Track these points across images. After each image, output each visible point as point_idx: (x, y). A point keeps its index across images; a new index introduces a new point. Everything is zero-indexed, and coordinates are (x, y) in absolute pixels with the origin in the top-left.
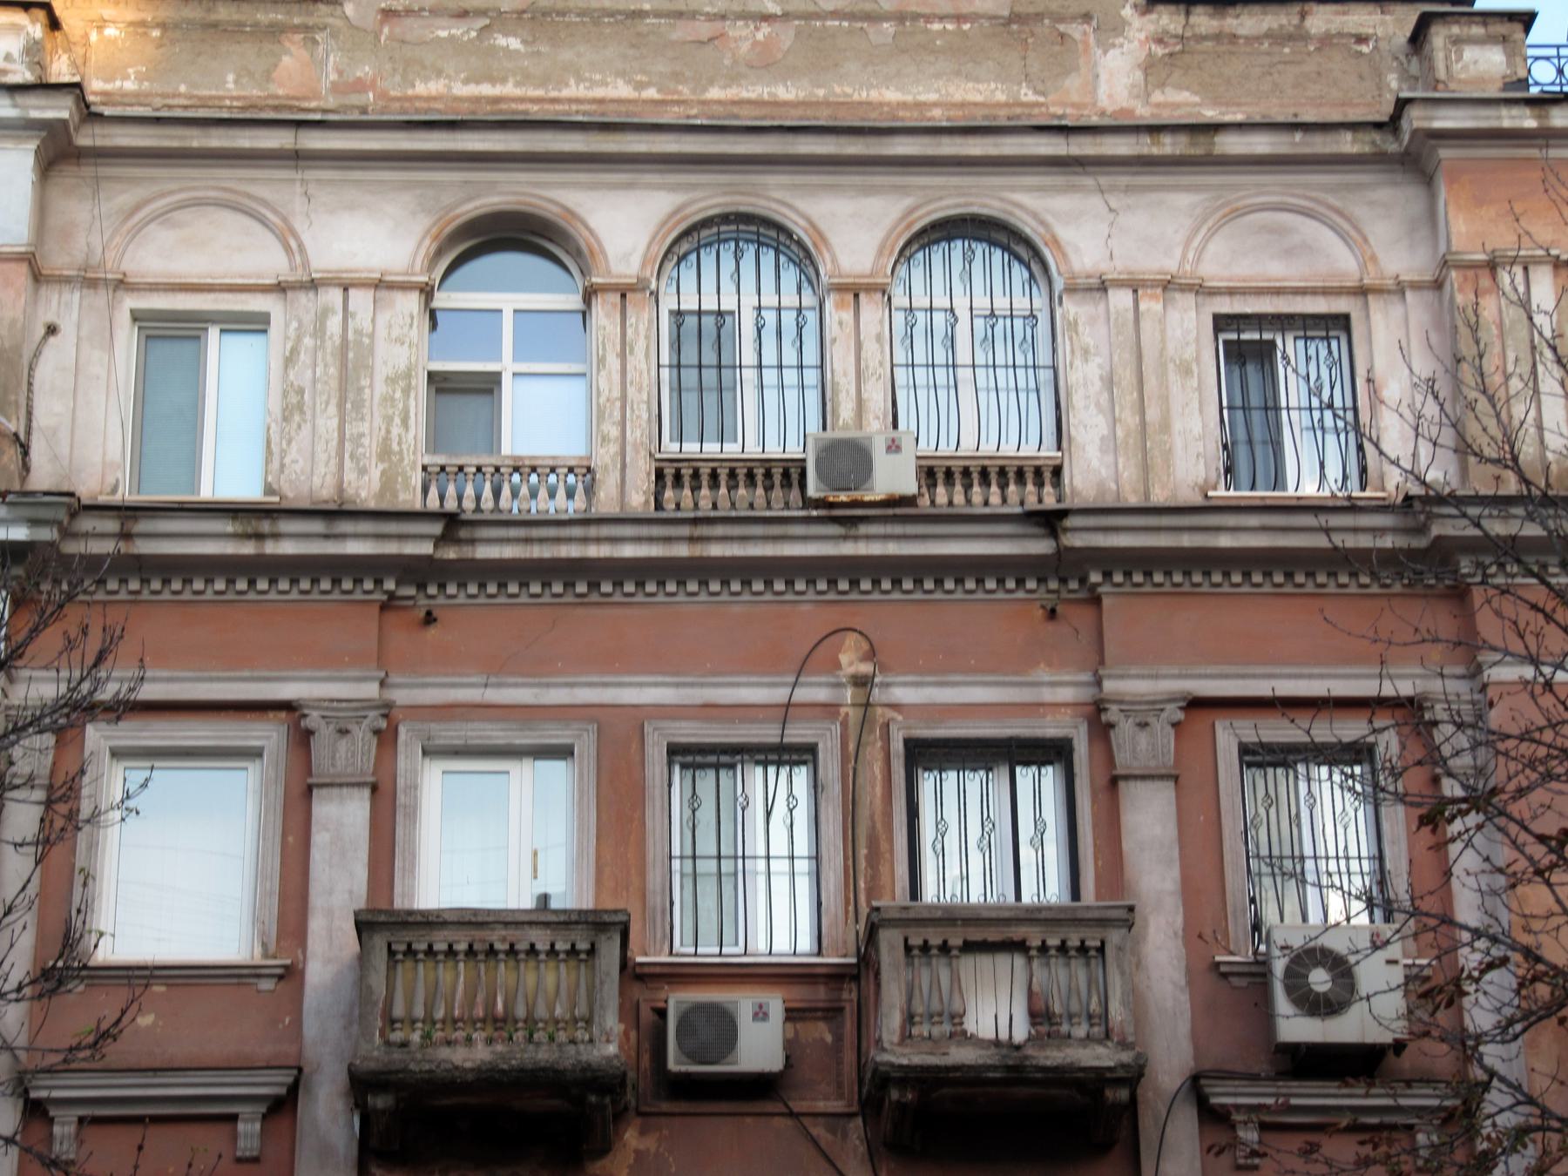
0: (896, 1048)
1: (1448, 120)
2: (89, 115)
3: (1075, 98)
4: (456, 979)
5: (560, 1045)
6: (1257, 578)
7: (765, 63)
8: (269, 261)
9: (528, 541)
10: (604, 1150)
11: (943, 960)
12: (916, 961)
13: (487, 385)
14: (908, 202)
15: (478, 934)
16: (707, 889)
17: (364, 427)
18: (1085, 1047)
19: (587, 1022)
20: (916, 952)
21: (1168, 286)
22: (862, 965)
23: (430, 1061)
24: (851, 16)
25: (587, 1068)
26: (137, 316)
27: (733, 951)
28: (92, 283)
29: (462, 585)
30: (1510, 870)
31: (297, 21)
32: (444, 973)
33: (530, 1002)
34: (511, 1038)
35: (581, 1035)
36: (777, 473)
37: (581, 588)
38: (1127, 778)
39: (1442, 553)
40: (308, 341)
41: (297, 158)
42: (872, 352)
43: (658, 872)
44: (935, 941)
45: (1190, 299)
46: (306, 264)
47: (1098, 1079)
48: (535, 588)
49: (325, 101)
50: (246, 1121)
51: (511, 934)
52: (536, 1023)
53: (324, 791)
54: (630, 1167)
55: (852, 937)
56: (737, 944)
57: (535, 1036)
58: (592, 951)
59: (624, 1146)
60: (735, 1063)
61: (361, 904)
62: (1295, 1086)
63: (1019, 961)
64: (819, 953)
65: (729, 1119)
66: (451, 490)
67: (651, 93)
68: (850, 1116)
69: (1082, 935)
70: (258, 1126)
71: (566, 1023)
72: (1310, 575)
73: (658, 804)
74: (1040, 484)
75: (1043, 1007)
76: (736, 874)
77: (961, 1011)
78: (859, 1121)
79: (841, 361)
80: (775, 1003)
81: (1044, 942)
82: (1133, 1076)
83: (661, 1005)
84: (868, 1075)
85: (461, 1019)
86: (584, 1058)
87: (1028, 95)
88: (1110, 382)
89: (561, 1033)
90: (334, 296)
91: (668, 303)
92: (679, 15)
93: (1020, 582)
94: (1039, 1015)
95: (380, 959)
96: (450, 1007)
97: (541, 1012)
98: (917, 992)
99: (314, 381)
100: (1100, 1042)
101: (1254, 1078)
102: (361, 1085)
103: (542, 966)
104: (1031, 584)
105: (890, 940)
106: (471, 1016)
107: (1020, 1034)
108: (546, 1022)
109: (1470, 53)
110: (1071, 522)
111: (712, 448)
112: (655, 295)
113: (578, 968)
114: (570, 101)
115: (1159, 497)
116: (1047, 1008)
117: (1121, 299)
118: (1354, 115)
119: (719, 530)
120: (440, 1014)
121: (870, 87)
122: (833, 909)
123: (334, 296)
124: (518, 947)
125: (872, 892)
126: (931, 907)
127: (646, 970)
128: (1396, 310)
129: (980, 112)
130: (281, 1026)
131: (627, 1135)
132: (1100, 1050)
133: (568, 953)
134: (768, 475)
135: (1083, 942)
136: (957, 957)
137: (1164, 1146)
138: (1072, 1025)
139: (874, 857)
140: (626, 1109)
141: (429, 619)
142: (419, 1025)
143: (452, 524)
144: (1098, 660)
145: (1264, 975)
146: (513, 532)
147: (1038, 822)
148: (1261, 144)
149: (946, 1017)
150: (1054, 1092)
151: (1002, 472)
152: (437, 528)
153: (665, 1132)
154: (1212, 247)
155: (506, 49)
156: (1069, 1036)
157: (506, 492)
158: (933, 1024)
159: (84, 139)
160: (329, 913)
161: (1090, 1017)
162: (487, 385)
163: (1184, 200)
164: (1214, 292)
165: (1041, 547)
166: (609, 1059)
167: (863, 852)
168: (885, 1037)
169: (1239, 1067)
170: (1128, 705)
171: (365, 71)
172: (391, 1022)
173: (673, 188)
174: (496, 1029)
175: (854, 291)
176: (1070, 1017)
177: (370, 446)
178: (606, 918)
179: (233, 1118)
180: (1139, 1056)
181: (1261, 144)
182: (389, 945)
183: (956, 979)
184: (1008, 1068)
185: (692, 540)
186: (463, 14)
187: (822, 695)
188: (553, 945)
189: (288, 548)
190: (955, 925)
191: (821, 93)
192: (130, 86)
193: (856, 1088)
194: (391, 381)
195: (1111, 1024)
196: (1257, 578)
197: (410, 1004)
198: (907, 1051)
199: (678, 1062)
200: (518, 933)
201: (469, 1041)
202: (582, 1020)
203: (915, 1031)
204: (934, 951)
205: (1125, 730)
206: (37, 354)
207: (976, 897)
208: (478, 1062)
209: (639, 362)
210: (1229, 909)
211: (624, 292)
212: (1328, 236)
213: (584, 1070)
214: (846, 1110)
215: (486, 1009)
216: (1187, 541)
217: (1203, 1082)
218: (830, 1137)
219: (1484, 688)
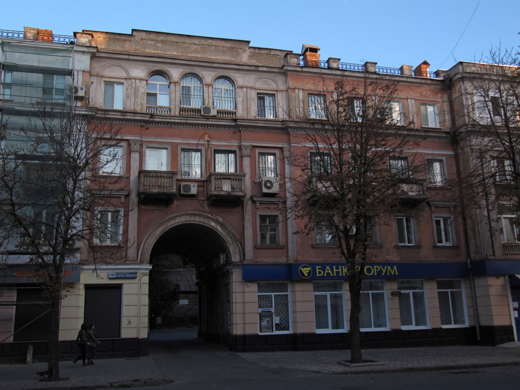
1: (290, 68)
2: (98, 51)
3: (239, 60)
4: (153, 180)
6: (262, 130)
7: (196, 51)
8: (124, 75)
9: (162, 118)
10: (172, 204)
13: (155, 95)
14: (216, 73)
15: (156, 174)
17: (138, 100)
21: (251, 88)
24: (208, 45)
25: (172, 193)
26: (104, 81)
28: (98, 76)
29: (152, 124)
30: (472, 147)
31: (128, 39)
32: (151, 179)
36: (197, 110)
37: (169, 126)
39: (287, 128)
40: (130, 87)
41: (128, 60)
42: (211, 95)
44: (219, 178)
45: (254, 90)
46: (129, 75)
47: (240, 197)
48: (163, 125)
49: (132, 51)
51: (161, 174)
58: (172, 177)
62: (264, 198)
63: (230, 181)
66: (150, 110)
67: (180, 54)
72: (269, 130)
74: (233, 115)
78: (206, 201)
79: (206, 95)
80: (196, 185)
82: (244, 196)
87: (233, 59)
88: (243, 101)
90: (134, 81)
91: (182, 85)
92: (184, 43)
93: (230, 128)
94: (232, 188)
97: (165, 185)
99: (131, 93)
101: (259, 197)
102: (139, 194)
104: (232, 129)
105: (213, 178)
107: (230, 190)
109: (292, 59)
110: (238, 121)
111: (188, 106)
112: (180, 84)
114: (168, 54)
115: (249, 118)
117: (245, 89)
118: (277, 66)
119: (189, 119)
121: (173, 52)
123: (134, 81)
126: (217, 173)
128: (281, 94)
129: (229, 61)
134: (195, 111)
139: (209, 166)
141: (147, 129)
143: (152, 115)
144: (240, 140)
146: (160, 117)
148: (264, 69)
151: (228, 112)
152: (149, 116)
154: (257, 83)
155: (159, 46)
157: (158, 111)
159: (97, 55)
162: (155, 95)
163: (253, 76)
164: (257, 89)
165: (234, 124)
167: (208, 164)
170: (244, 146)
171: (138, 47)
172: (144, 185)
173: (182, 68)
175: (208, 85)
177: (139, 103)
179: (120, 197)
181: (264, 69)
183: (221, 183)
185: (185, 120)
186: (153, 40)
187: (202, 142)
189: (128, 117)
191: (204, 56)
192: (103, 47)
194: (142, 94)
196: (262, 130)
197: (147, 183)
201: (155, 188)
205: (244, 149)
206: (90, 86)
209: (177, 93)
211: (175, 83)
212: (273, 83)
216: (253, 124)
219: (291, 146)
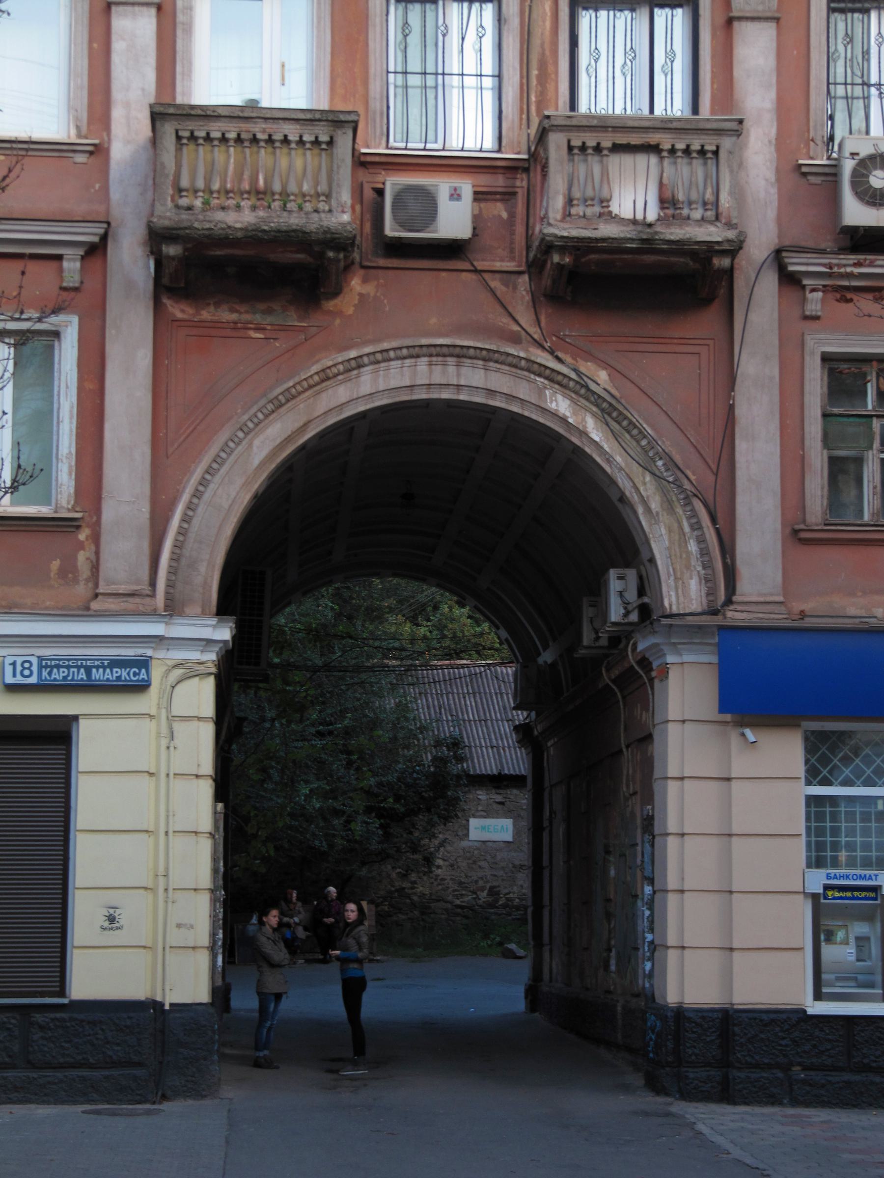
0: (559, 224)
5: (307, 213)
10: (336, 292)
11: (596, 158)
12: (576, 158)
15: (244, 126)
16: (415, 95)
18: (700, 226)
19: (327, 197)
20: (576, 151)
22: (532, 160)
23: (210, 222)
25: (328, 231)
27: (434, 147)
32: (219, 154)
33: (284, 181)
34: (269, 207)
35: (322, 206)
38: (740, 19)
43: (378, 83)
47: (710, 250)
50: (69, 260)
51: (270, 127)
52: (288, 195)
53: (121, 8)
54: (355, 306)
55: (525, 138)
56: (436, 142)
57: (288, 205)
58: (331, 143)
59: (351, 290)
60: (435, 231)
61: (152, 100)
63: (654, 159)
64: (499, 151)
65: (428, 273)
68: (520, 273)
69: (702, 142)
70: (78, 265)
71: (311, 196)
73: (378, 29)
75: (670, 196)
76: (436, 87)
77: (609, 197)
78: (526, 277)
80: (467, 187)
81: (673, 146)
82: (734, 249)
83: (380, 186)
84: (536, 243)
85: (232, 191)
86: (325, 223)
89: (308, 204)
94: (667, 201)
95: (169, 141)
96: (224, 181)
97: (292, 188)
98: (576, 181)
100: (711, 222)
103: (278, 151)
105: (556, 142)
106: (239, 189)
107: (652, 216)
108: (296, 195)
113: (320, 155)
116: (673, 196)
120: (216, 186)
122: (510, 116)
124: (274, 137)
125: (540, 104)
126: (586, 116)
127: (369, 159)
130: (92, 190)
131: (353, 283)
132: (712, 229)
133: (312, 143)
135: (702, 146)
136: (607, 156)
137: (752, 302)
138: (691, 209)
139: (543, 78)
140: (353, 263)
142: (201, 194)
145: (835, 175)
147: (670, 56)
149: (596, 202)
150: (673, 259)
153: (382, 281)
156: (688, 218)
158: (587, 206)
160: (127, 105)
161: (705, 204)
166: (344, 225)
167: (535, 72)
168: (551, 215)
169: (810, 244)
174: (259, 199)
176: (690, 203)
178: (342, 117)
179: (59, 258)
180: (741, 232)
182: (177, 131)
183: (605, 173)
184: (643, 241)
188: (301, 137)
190: (607, 131)
193: (524, 253)
195: (721, 209)
198: (566, 226)
199: (393, 230)
200: (275, 126)
201: (238, 207)
202: (323, 195)
203: (574, 211)
204: (590, 151)
207: (619, 111)
208: (246, 224)
210: (812, 124)
213: (325, 232)
214: (517, 269)
215: (251, 184)
217: (784, 254)
218: (504, 288)
